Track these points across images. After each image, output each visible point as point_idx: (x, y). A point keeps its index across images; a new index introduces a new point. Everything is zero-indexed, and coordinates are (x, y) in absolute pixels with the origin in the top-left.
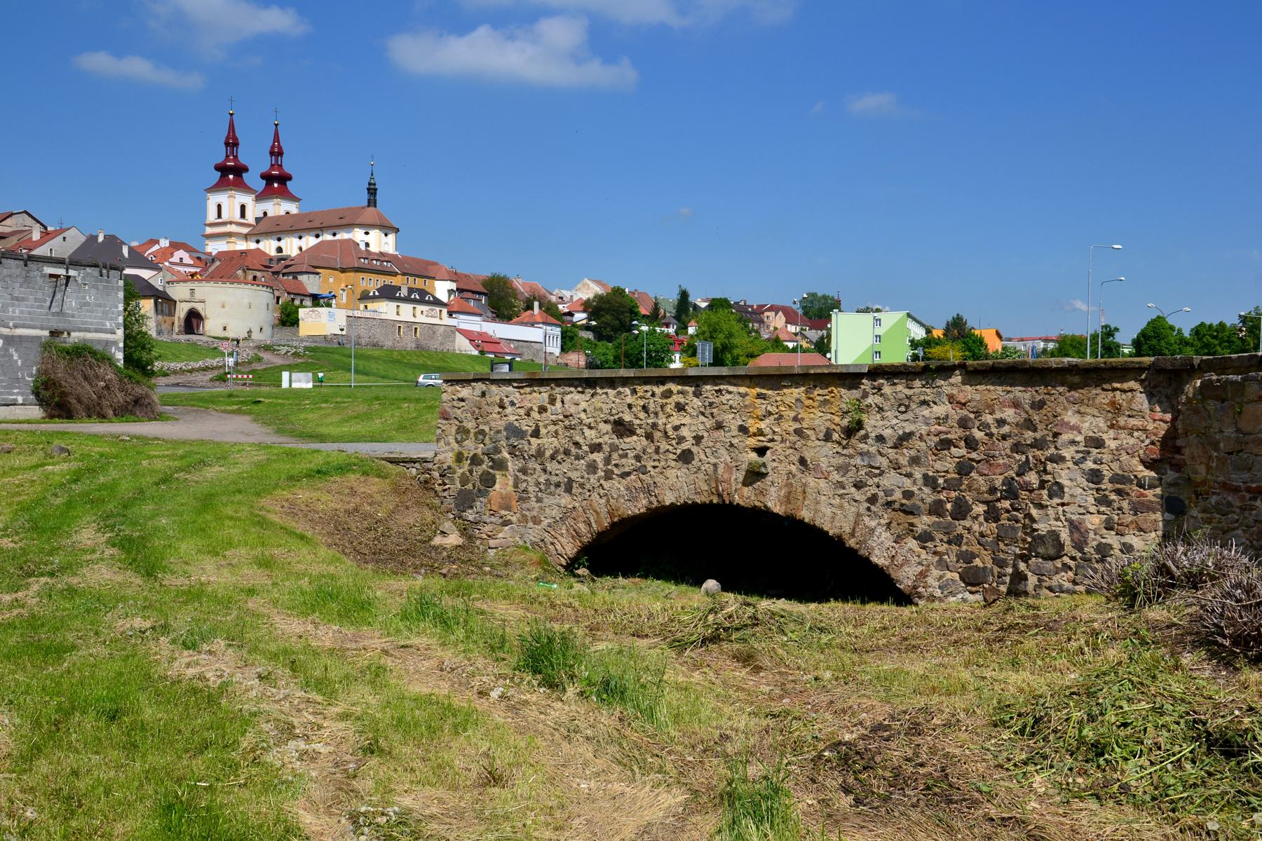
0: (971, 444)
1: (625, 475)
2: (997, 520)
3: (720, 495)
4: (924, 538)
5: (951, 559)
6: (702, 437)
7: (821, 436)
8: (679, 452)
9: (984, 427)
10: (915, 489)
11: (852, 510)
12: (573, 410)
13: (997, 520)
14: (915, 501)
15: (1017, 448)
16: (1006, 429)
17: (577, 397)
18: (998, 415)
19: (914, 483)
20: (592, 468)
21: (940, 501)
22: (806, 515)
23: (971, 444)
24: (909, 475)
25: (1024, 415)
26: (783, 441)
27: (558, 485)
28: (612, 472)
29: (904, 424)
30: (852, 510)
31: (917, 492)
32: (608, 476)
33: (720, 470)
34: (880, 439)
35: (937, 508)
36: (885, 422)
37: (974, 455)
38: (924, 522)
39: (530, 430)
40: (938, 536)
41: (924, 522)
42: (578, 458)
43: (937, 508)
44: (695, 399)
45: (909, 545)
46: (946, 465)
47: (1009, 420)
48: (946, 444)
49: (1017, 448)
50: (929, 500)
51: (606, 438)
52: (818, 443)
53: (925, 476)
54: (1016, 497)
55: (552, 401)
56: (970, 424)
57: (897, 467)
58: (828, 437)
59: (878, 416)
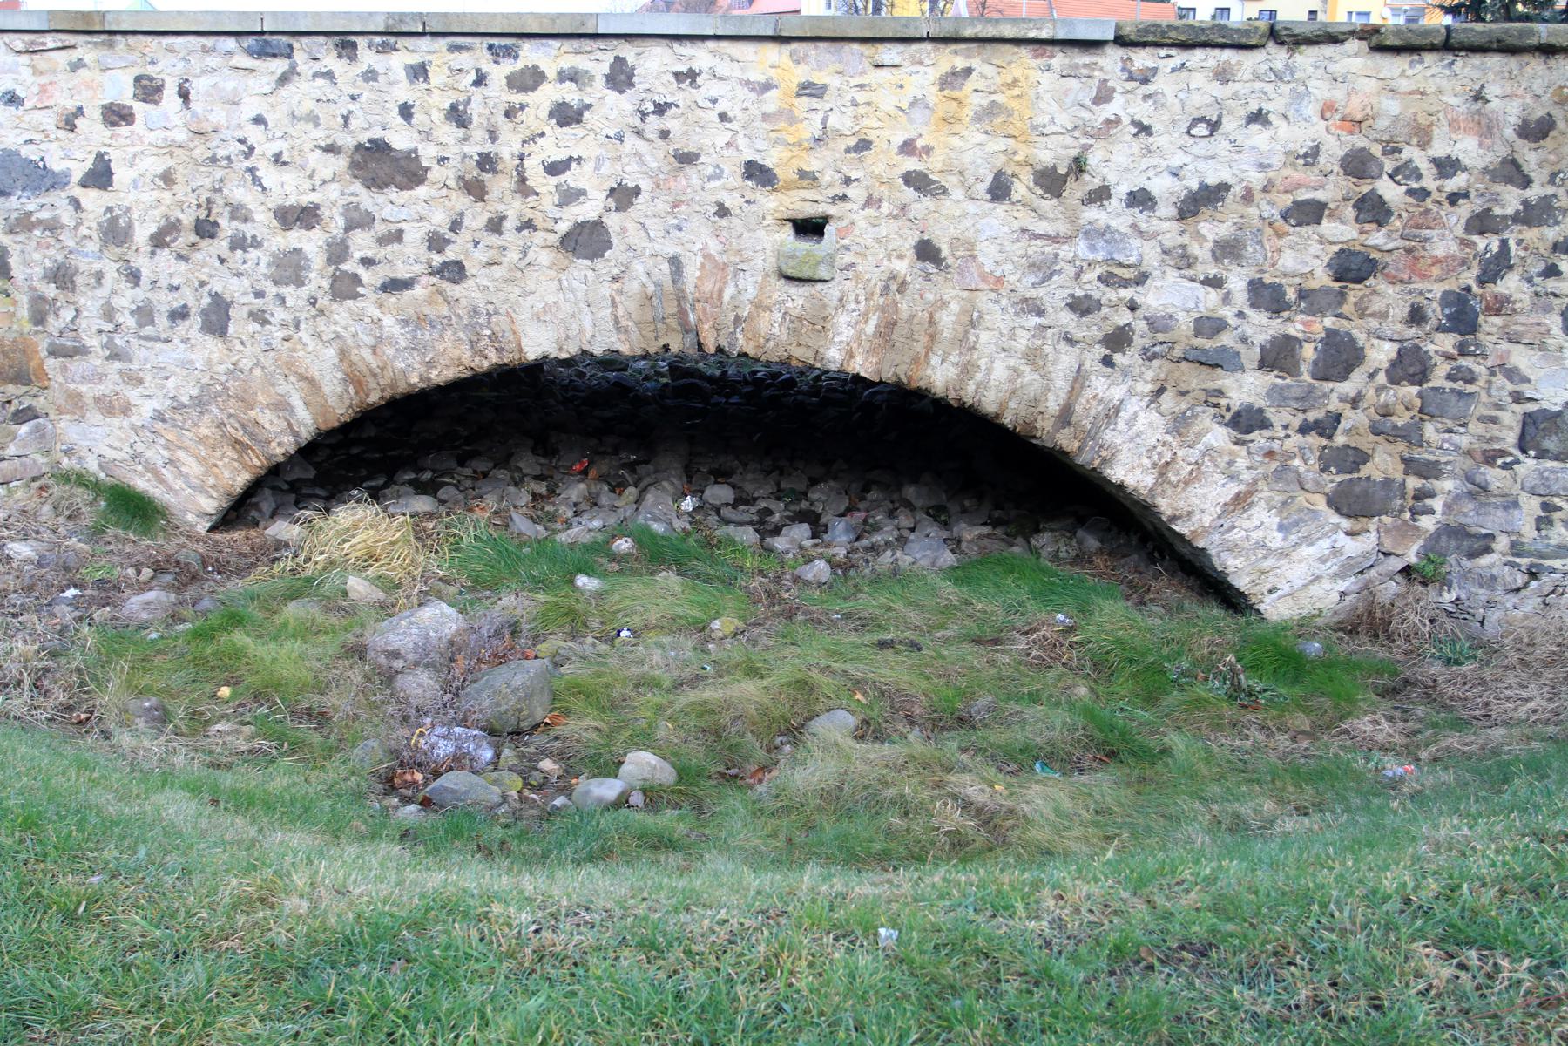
0: (1373, 210)
1: (395, 286)
2: (1421, 377)
3: (686, 329)
4: (1246, 422)
5: (1305, 467)
6: (637, 191)
7: (981, 189)
8: (563, 227)
9: (1404, 172)
10: (1228, 313)
11: (1066, 360)
12: (218, 116)
13: (1421, 377)
14: (1226, 339)
15: (1482, 223)
16: (1457, 182)
17: (230, 83)
18: (1439, 149)
19: (1227, 299)
20: (290, 268)
21: (1288, 339)
22: (939, 376)
23: (1373, 210)
24: (1215, 282)
25: (1503, 152)
26: (869, 202)
27: (179, 315)
28: (356, 279)
29: (1201, 165)
30: (1066, 360)
31: (1233, 321)
32: (344, 288)
33: (691, 273)
34: (1141, 199)
35: (1278, 356)
36: (1153, 161)
37: (1378, 238)
38: (1247, 387)
39: (78, 171)
40: (1278, 417)
41: (1247, 387)
42: (239, 243)
43: (1278, 356)
44: (612, 95)
45: (1209, 439)
46: (1304, 258)
47: (1465, 160)
48: (1309, 213)
49: (1482, 223)
50: (1260, 338)
51: (333, 191)
52: (971, 207)
53: (1255, 287)
54: (1472, 328)
55: (149, 90)
56: (1374, 169)
57: (1184, 261)
58: (1000, 190)
59: (1136, 146)
